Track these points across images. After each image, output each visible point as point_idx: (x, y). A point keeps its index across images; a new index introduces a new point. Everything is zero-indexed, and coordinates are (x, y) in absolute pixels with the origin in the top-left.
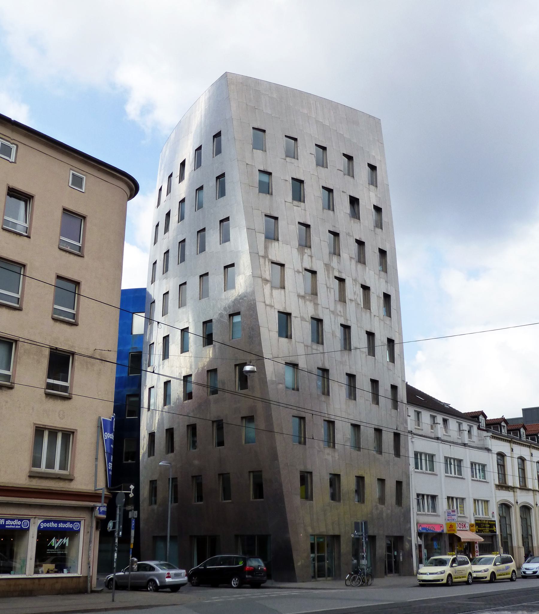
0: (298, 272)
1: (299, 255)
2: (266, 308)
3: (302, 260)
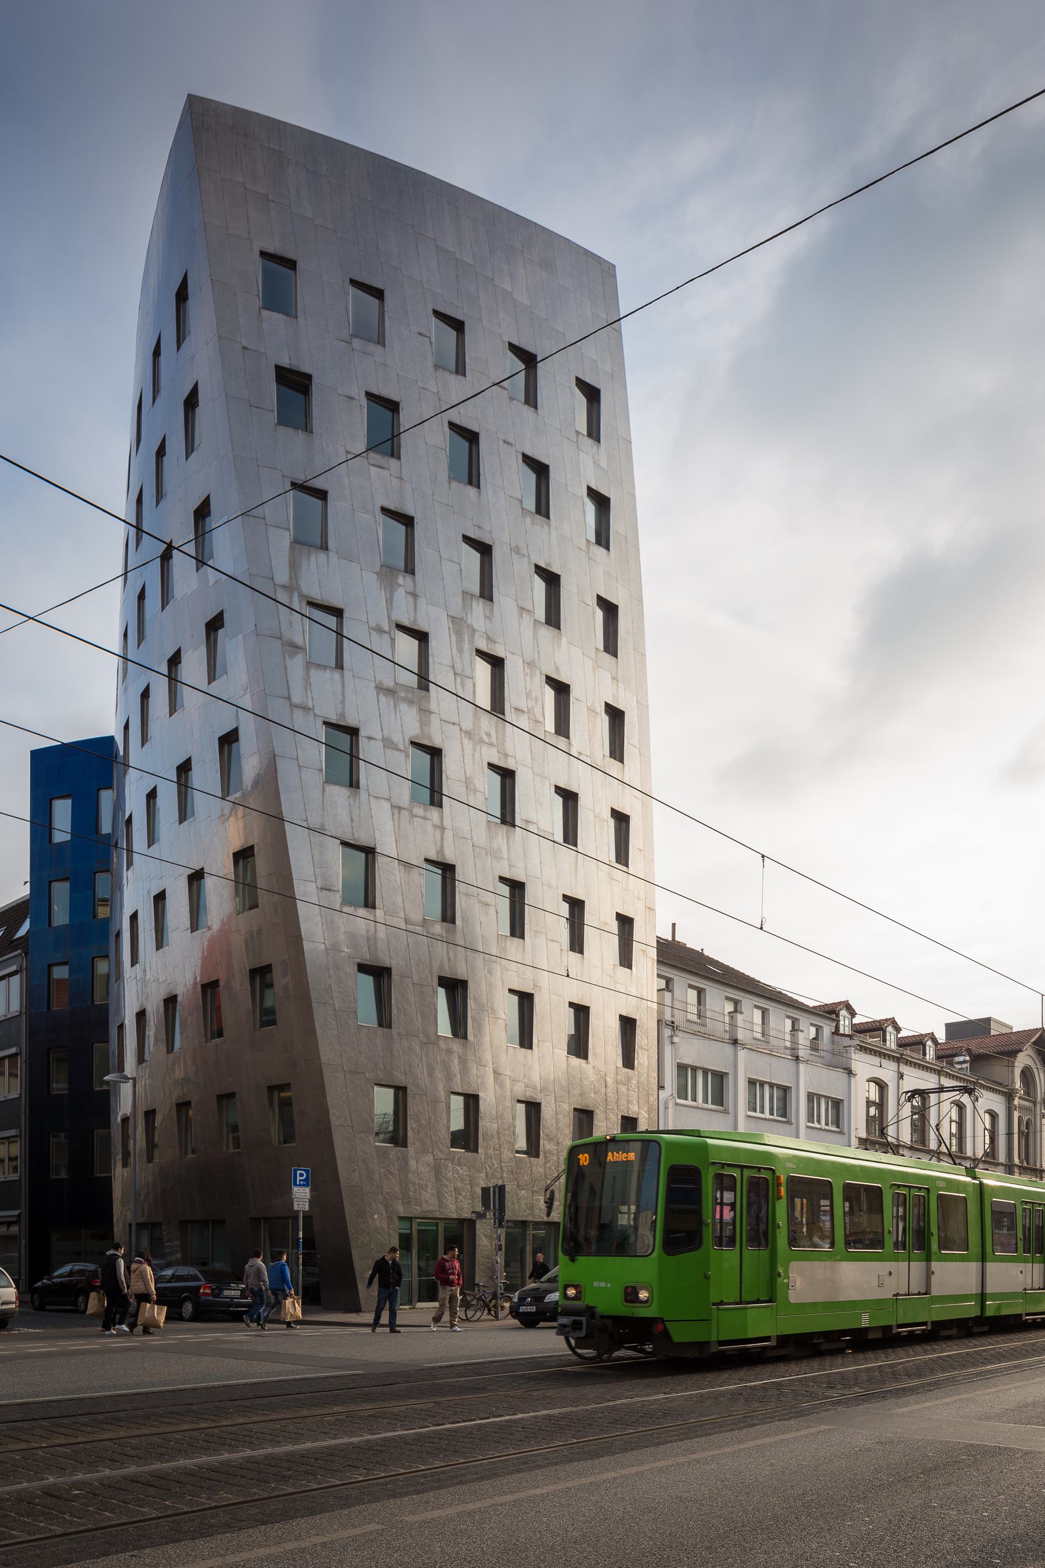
0: (380, 631)
2: (292, 712)
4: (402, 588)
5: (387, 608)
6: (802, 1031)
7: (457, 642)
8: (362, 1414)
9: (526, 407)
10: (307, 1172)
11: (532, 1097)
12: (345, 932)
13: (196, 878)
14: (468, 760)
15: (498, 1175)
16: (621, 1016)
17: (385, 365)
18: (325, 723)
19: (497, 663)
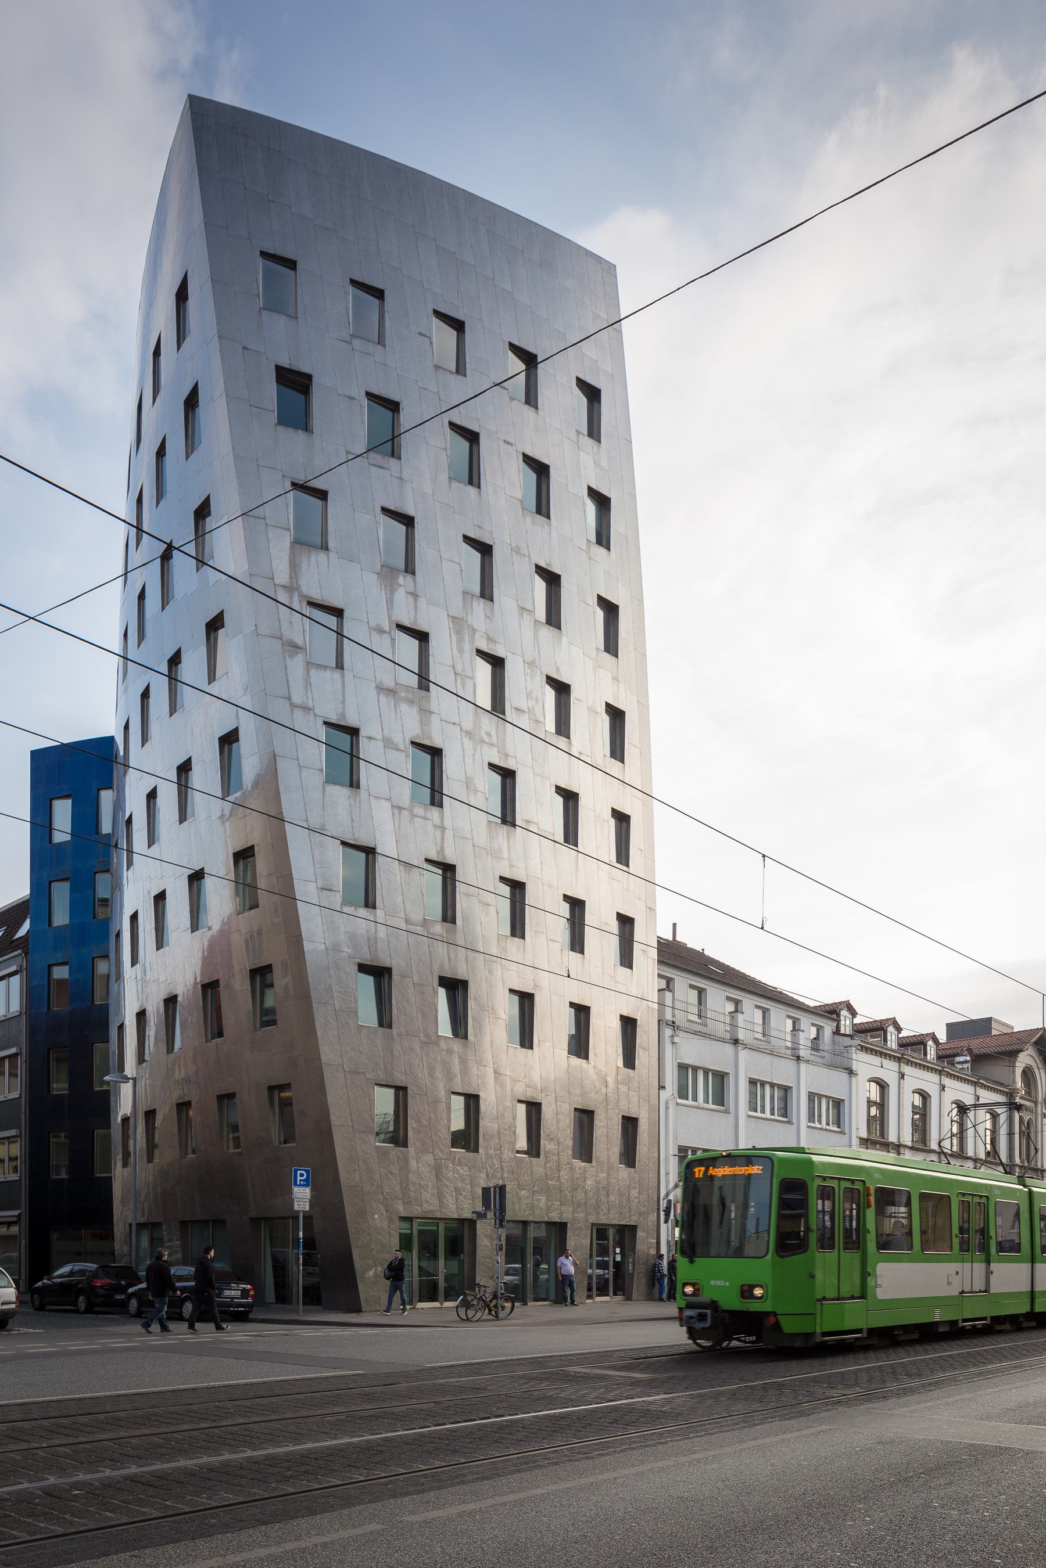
1: (383, 591)
5: (388, 609)
6: (803, 1031)
7: (457, 642)
8: (362, 1414)
9: (527, 406)
10: (307, 1172)
12: (346, 933)
13: (196, 878)
15: (499, 1175)
17: (385, 365)
18: (325, 723)
19: (497, 663)
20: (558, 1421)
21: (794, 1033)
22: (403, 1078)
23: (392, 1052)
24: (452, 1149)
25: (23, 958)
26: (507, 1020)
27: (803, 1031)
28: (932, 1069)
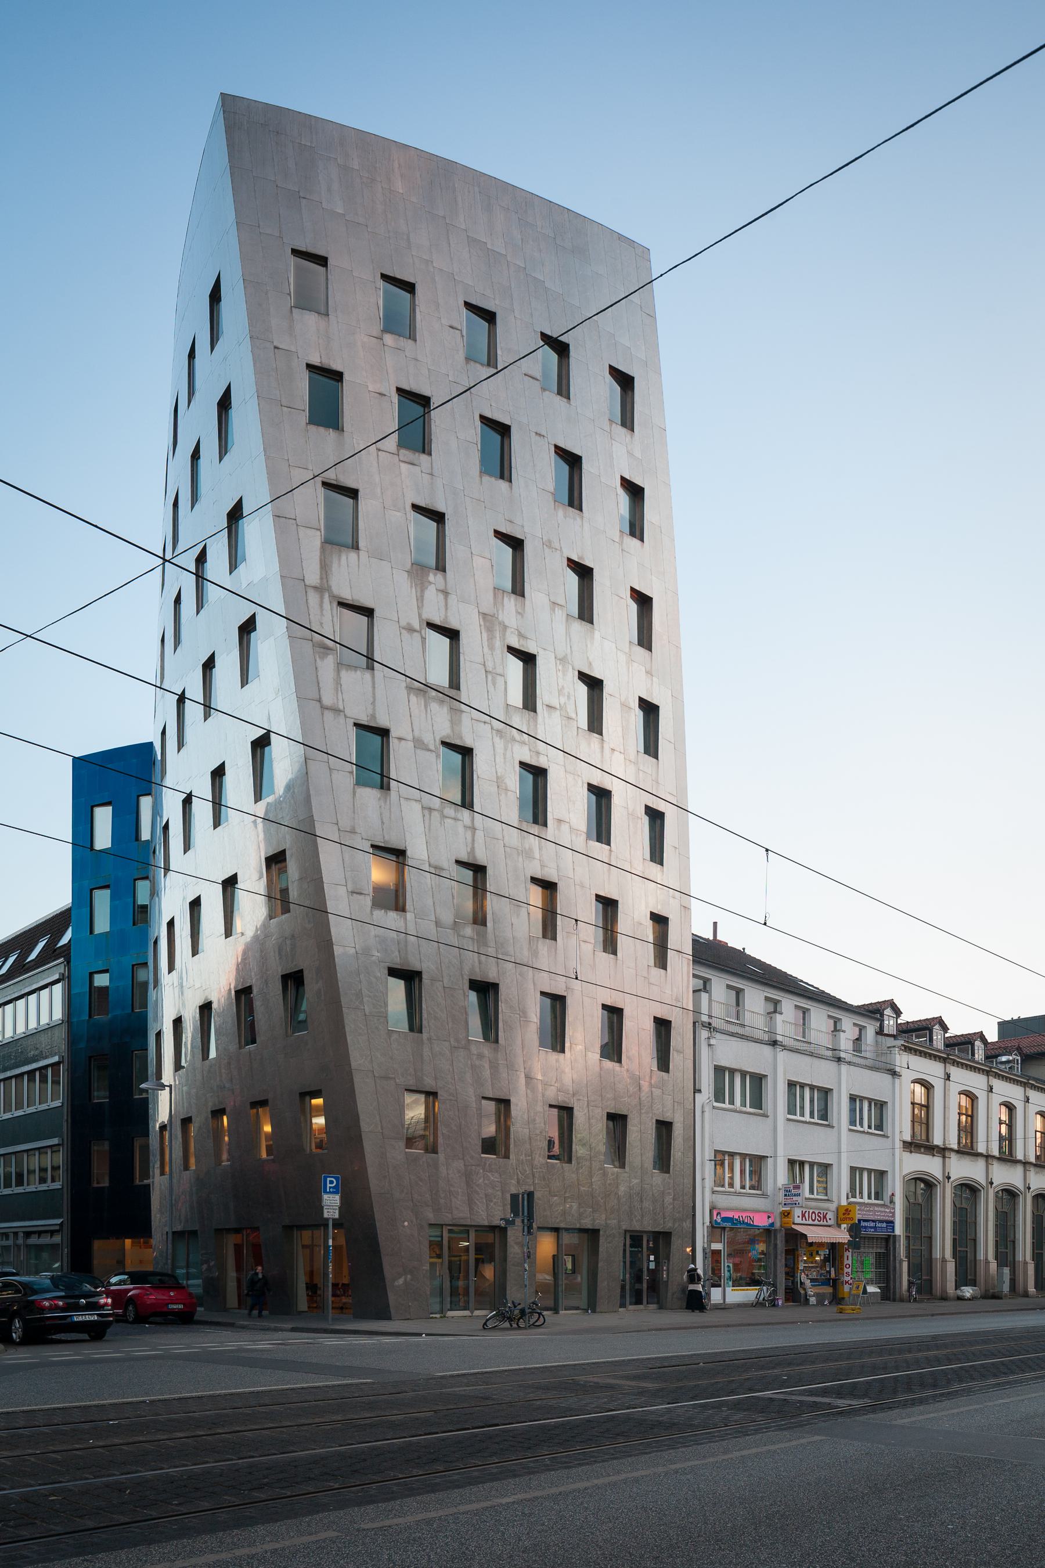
0: (410, 630)
1: (414, 589)
2: (323, 714)
3: (419, 601)
4: (433, 585)
5: (418, 607)
6: (844, 1031)
7: (488, 640)
8: (359, 1422)
9: (559, 397)
10: (337, 1179)
11: (564, 1102)
12: (375, 936)
13: (230, 883)
14: (499, 759)
15: (530, 1181)
16: (655, 1018)
17: (416, 360)
18: (355, 724)
19: (528, 659)
20: (549, 1430)
21: (834, 1033)
22: (433, 1083)
23: (422, 1056)
24: (483, 1155)
25: (65, 966)
26: (539, 1024)
27: (844, 1031)
28: (979, 1069)
